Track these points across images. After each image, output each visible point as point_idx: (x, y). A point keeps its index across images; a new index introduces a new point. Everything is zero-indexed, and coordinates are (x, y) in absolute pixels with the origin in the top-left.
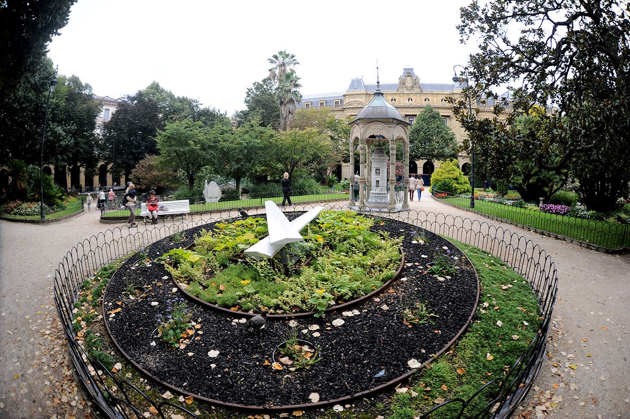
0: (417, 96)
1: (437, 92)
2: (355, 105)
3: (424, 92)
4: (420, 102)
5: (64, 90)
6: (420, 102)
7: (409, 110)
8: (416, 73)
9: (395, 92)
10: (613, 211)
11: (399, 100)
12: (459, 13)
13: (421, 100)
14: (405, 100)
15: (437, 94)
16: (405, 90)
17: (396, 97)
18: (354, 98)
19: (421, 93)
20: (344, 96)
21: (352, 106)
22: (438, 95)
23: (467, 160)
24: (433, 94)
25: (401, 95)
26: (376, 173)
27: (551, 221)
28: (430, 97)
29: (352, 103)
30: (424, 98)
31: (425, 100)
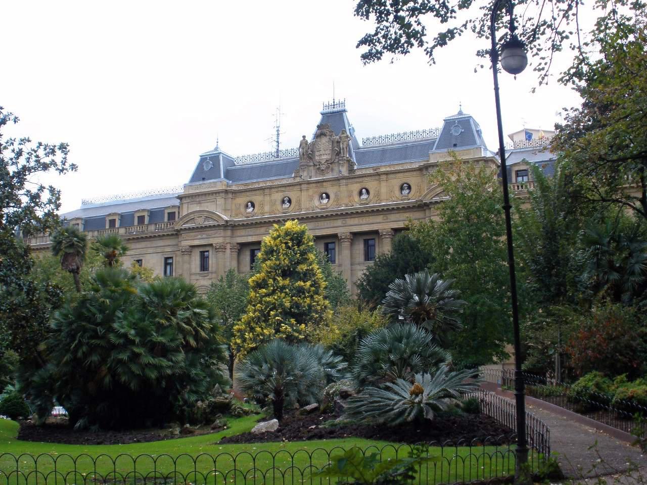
0: (379, 180)
1: (388, 169)
2: (200, 222)
3: (358, 173)
4: (346, 201)
5: (632, 426)
6: (346, 201)
7: (322, 224)
9: (291, 181)
10: (169, 422)
11: (299, 202)
12: (65, 141)
13: (273, 203)
14: (311, 198)
15: (387, 174)
16: (313, 173)
17: (293, 194)
18: (200, 203)
19: (352, 176)
20: (180, 198)
21: (193, 225)
22: (391, 176)
23: (312, 371)
24: (378, 174)
25: (304, 186)
27: (59, 477)
28: (371, 185)
29: (192, 216)
30: (356, 187)
31: (361, 193)
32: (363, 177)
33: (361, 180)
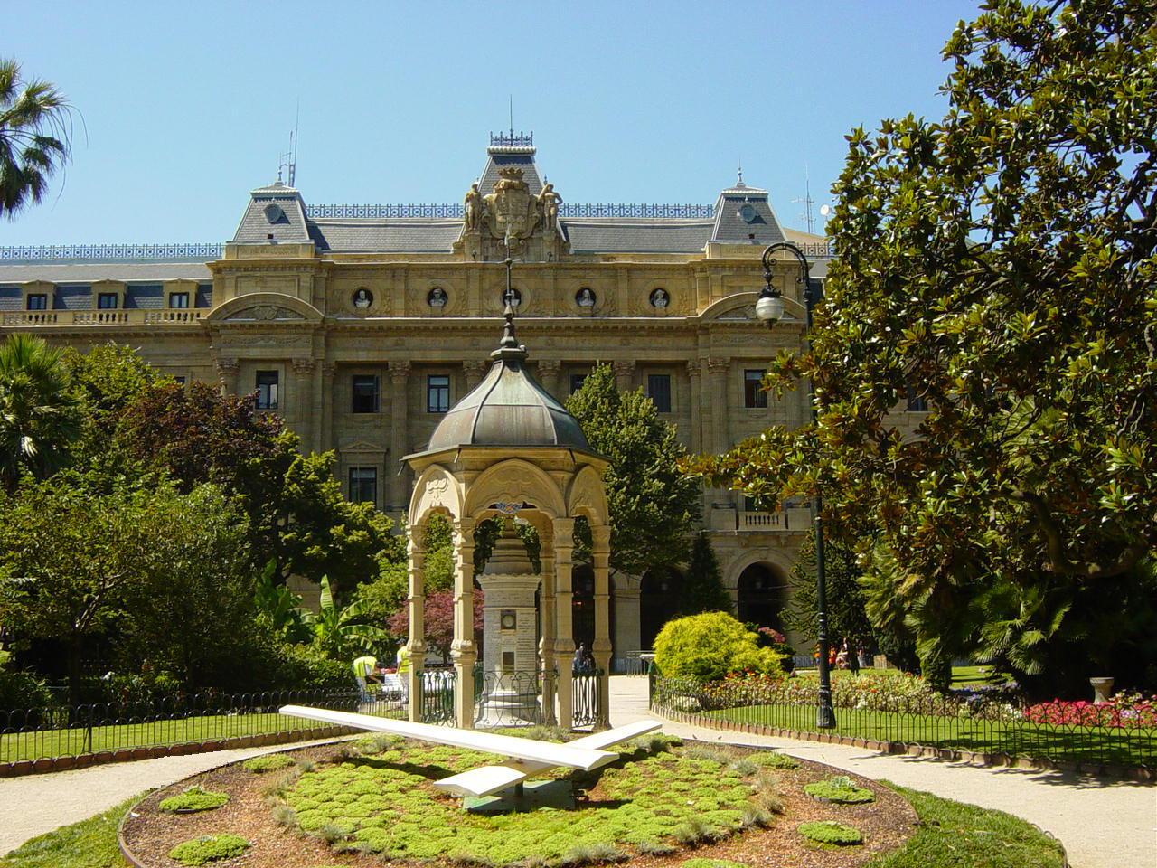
8: (549, 170)
26: (503, 627)
32: (585, 269)
33: (581, 273)
